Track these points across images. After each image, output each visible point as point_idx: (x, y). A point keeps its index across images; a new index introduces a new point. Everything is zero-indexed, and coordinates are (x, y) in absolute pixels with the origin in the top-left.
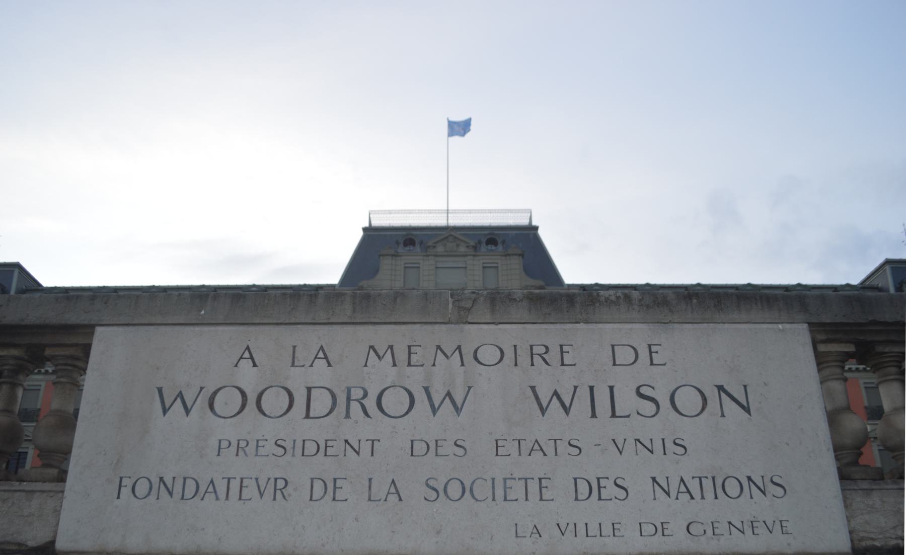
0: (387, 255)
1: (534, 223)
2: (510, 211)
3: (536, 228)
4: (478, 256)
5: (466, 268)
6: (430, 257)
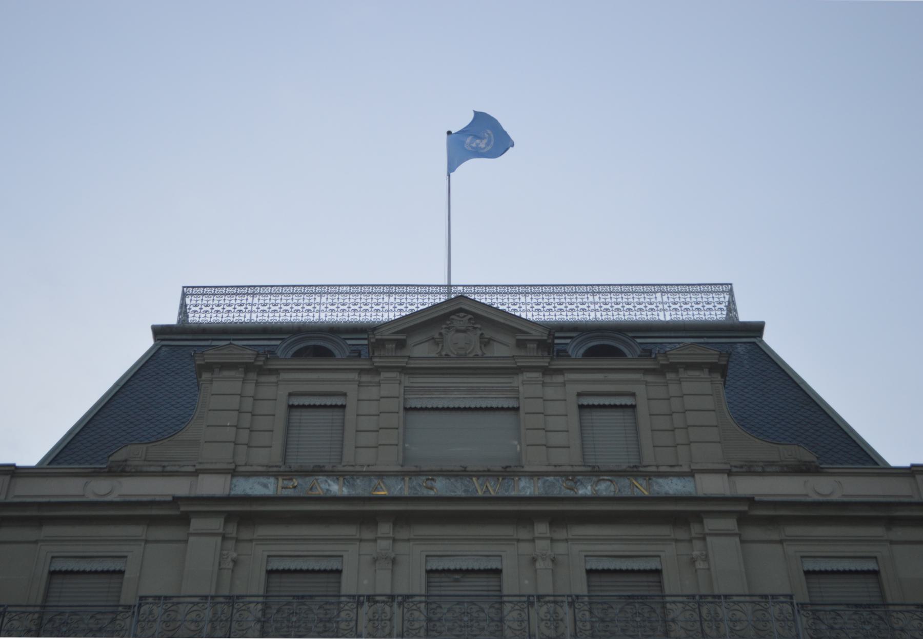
0: (224, 366)
1: (745, 315)
2: (661, 288)
3: (757, 329)
4: (560, 371)
5: (516, 409)
6: (384, 375)
